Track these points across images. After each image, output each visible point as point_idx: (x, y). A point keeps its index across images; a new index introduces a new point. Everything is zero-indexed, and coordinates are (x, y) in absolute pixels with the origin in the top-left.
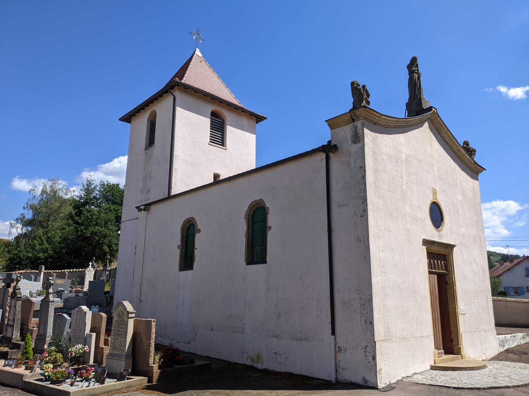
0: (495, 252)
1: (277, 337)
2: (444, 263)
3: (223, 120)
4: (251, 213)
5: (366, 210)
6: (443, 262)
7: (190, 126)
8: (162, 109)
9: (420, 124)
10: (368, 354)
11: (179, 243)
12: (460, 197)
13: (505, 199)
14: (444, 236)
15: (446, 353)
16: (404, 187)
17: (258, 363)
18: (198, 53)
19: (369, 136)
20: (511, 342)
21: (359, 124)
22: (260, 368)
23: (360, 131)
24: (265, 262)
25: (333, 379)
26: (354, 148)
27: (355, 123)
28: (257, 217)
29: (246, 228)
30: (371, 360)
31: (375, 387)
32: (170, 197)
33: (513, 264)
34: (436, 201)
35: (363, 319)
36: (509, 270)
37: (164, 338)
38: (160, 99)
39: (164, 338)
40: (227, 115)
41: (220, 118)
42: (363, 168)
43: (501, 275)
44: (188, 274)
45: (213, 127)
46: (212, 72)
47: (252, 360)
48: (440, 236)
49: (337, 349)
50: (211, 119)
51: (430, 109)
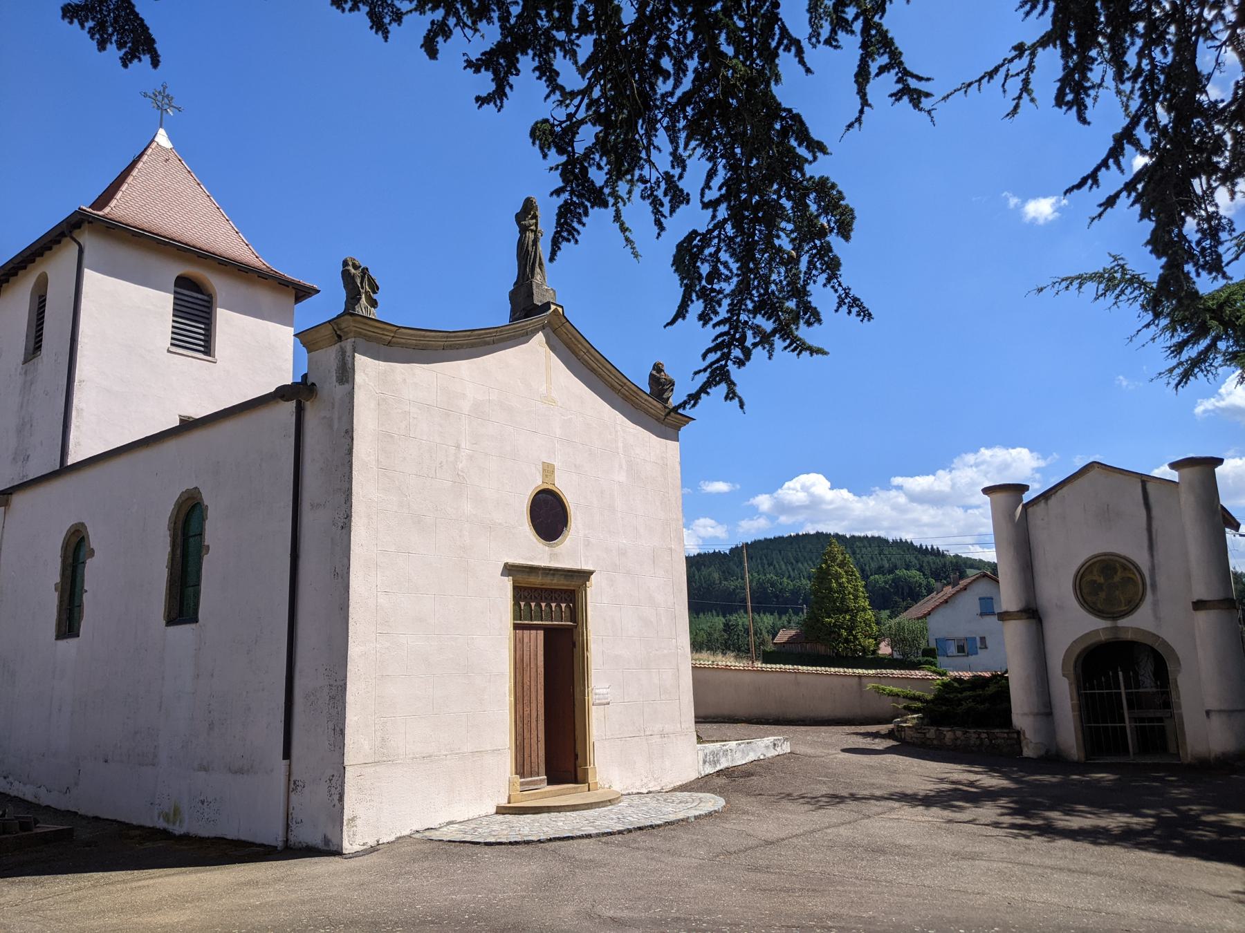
0: (981, 561)
1: (205, 769)
2: (568, 606)
3: (210, 296)
4: (182, 516)
5: (349, 517)
6: (563, 605)
7: (120, 314)
8: (59, 266)
9: (525, 337)
10: (333, 790)
11: (58, 580)
12: (622, 477)
13: (1010, 444)
14: (563, 555)
15: (550, 782)
16: (460, 466)
17: (174, 824)
18: (162, 139)
19: (367, 369)
20: (738, 755)
21: (348, 344)
22: (177, 833)
23: (350, 359)
24: (196, 620)
25: (280, 844)
26: (340, 390)
27: (343, 343)
28: (188, 521)
29: (169, 549)
30: (336, 802)
31: (338, 853)
32: (64, 470)
33: (957, 588)
34: (550, 487)
35: (331, 725)
36: (946, 601)
37: (25, 784)
38: (55, 247)
39: (25, 784)
40: (218, 284)
41: (197, 293)
42: (349, 433)
43: (929, 613)
44: (183, 631)
45: (180, 310)
46: (193, 183)
47: (167, 818)
48: (553, 556)
49: (292, 785)
50: (175, 292)
51: (547, 306)
